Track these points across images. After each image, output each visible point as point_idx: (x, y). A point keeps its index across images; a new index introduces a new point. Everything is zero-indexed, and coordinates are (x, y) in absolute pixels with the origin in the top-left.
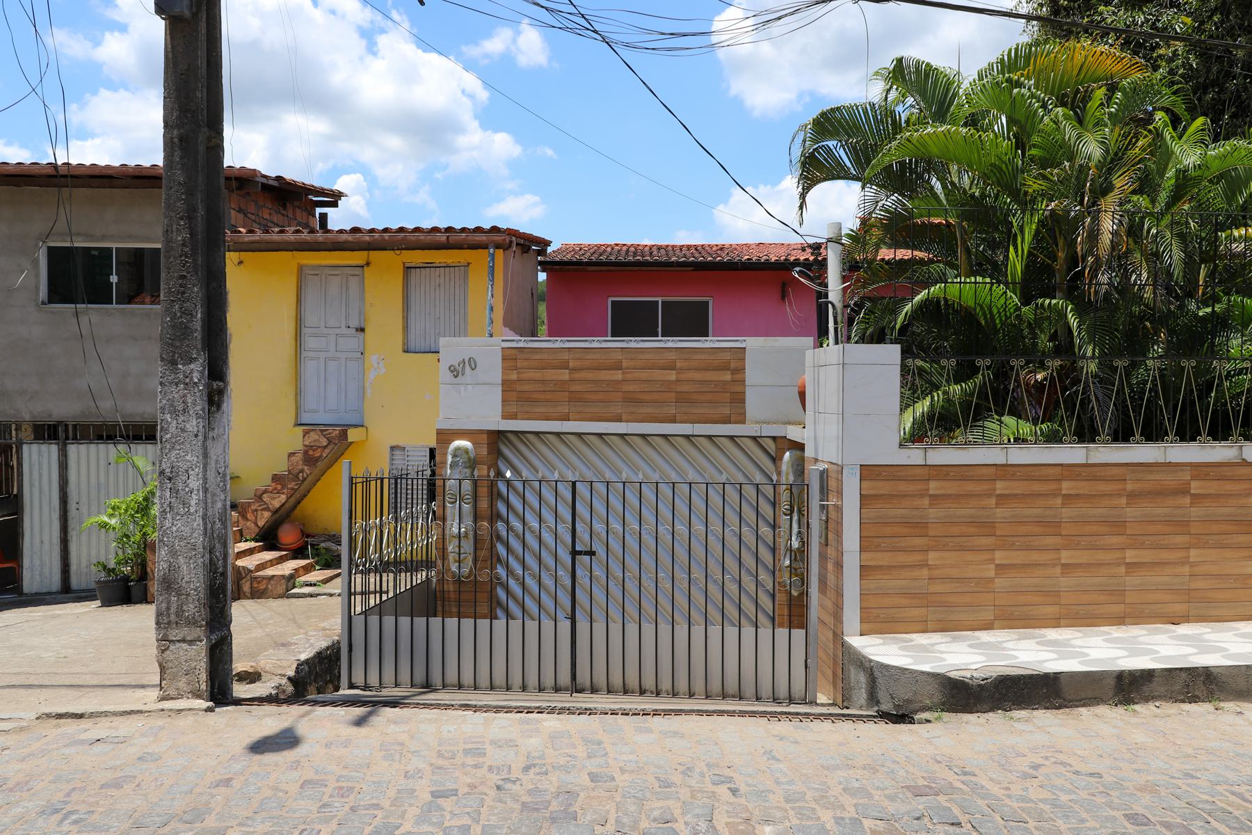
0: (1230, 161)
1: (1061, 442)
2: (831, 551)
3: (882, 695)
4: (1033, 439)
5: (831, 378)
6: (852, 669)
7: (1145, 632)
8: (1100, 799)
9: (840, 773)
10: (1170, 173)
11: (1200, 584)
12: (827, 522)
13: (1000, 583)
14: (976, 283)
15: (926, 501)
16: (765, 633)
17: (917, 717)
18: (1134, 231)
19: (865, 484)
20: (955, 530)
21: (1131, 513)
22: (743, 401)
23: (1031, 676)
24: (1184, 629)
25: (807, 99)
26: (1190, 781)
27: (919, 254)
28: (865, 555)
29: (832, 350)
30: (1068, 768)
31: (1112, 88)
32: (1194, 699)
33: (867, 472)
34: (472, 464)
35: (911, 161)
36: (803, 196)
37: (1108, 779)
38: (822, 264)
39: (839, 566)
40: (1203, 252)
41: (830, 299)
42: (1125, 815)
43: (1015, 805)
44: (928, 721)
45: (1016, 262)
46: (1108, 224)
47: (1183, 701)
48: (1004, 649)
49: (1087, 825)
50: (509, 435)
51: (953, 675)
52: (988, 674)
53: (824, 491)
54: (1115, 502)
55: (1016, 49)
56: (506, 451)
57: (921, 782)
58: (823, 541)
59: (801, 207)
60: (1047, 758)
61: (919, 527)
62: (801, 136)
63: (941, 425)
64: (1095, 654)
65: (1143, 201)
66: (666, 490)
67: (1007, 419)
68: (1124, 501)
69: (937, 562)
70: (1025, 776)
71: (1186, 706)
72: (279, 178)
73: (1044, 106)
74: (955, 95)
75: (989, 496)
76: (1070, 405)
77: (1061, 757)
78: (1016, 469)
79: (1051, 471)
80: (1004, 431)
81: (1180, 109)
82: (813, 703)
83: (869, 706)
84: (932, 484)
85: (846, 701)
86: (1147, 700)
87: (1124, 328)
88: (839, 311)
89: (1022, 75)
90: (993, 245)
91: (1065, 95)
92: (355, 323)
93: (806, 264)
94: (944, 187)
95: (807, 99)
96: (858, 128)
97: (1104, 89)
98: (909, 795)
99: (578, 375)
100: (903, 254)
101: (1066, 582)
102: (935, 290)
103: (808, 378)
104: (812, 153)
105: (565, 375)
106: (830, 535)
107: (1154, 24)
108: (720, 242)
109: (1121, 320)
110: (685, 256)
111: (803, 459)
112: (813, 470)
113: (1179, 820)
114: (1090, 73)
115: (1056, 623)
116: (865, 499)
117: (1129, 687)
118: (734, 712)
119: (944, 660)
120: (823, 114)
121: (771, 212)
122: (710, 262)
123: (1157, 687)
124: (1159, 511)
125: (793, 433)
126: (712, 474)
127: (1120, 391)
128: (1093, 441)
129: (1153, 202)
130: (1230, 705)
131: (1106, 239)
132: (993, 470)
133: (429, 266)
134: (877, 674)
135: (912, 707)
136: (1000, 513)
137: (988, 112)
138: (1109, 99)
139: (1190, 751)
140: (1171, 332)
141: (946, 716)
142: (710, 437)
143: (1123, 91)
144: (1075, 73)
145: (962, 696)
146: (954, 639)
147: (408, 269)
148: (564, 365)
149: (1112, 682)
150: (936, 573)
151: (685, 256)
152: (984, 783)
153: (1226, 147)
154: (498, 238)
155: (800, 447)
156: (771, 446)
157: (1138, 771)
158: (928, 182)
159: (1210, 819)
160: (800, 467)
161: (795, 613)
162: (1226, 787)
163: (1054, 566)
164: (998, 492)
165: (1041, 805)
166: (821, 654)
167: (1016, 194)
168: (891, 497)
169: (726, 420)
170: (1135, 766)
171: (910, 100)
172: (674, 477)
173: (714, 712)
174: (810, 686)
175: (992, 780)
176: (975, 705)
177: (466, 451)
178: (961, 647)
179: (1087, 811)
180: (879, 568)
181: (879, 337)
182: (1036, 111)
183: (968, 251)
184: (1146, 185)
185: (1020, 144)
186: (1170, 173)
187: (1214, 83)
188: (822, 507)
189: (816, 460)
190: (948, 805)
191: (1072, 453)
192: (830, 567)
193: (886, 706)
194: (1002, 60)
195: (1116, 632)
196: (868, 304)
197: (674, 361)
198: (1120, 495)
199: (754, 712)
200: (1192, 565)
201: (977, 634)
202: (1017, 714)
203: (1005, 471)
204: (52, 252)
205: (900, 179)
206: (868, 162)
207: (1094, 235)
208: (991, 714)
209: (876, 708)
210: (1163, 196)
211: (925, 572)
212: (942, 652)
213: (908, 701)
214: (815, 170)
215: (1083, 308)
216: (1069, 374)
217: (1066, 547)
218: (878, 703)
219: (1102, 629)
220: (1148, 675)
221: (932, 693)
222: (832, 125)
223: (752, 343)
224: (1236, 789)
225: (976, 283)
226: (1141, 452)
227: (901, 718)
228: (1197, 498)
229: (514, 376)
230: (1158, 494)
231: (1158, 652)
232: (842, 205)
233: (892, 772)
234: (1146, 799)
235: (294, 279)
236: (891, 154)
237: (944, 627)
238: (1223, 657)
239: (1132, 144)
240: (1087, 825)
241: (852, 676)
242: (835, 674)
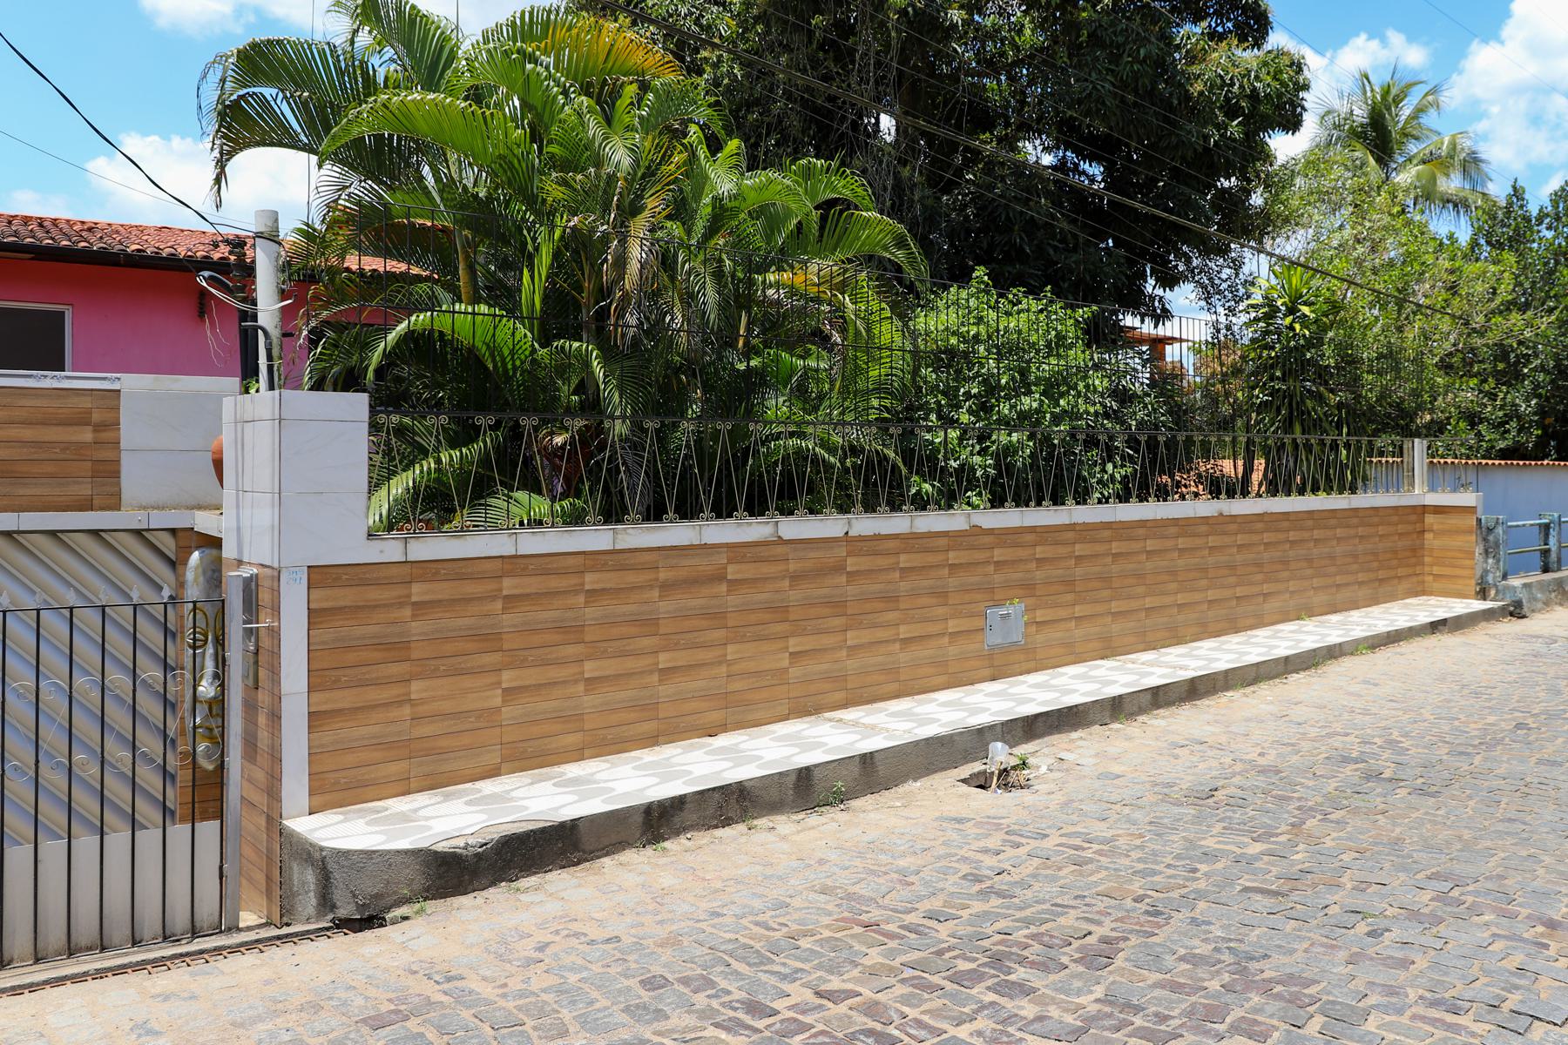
0: (767, 196)
1: (583, 523)
2: (263, 697)
3: (339, 895)
4: (550, 520)
5: (261, 440)
6: (295, 867)
7: (679, 751)
8: (615, 969)
9: (261, 1027)
10: (707, 200)
11: (737, 685)
12: (256, 653)
14: (474, 314)
17: (388, 916)
18: (667, 261)
19: (316, 594)
21: (665, 606)
22: (116, 474)
23: (543, 830)
24: (722, 740)
25: (252, 18)
26: (716, 920)
27: (415, 271)
28: (316, 697)
29: (263, 398)
30: (583, 939)
31: (644, 87)
32: (727, 822)
33: (319, 576)
35: (391, 136)
36: (221, 164)
37: (627, 940)
38: (249, 270)
39: (275, 717)
40: (739, 298)
41: (260, 322)
42: (641, 982)
43: (511, 1005)
44: (406, 918)
45: (531, 288)
46: (636, 253)
47: (716, 827)
48: (512, 800)
49: (597, 1005)
51: (440, 847)
52: (489, 837)
53: (251, 606)
54: (647, 595)
55: (531, 13)
57: (386, 1007)
58: (250, 682)
59: (218, 181)
60: (557, 932)
61: (397, 648)
62: (214, 77)
63: (433, 506)
64: (621, 787)
65: (676, 229)
66: (55, 624)
67: (521, 495)
68: (656, 593)
69: (424, 695)
70: (529, 962)
71: (719, 832)
73: (565, 93)
74: (452, 57)
76: (594, 473)
77: (576, 927)
78: (439, 566)
79: (571, 561)
80: (513, 509)
81: (717, 128)
82: (234, 928)
83: (320, 914)
84: (589, 577)
85: (286, 913)
86: (677, 833)
87: (659, 382)
88: (275, 341)
89: (538, 48)
90: (505, 265)
91: (590, 84)
93: (221, 266)
94: (438, 179)
95: (252, 18)
96: (310, 73)
97: (635, 86)
98: (365, 1030)
100: (373, 263)
102: (421, 319)
103: (227, 439)
104: (237, 102)
106: (262, 673)
107: (698, 19)
108: (89, 218)
109: (657, 368)
110: (16, 234)
111: (220, 558)
112: (234, 576)
113: (699, 971)
114: (618, 63)
115: (578, 754)
116: (315, 616)
117: (658, 822)
118: (86, 974)
119: (430, 828)
120: (254, 46)
121: (160, 182)
122: (65, 248)
123: (689, 816)
124: (460, 622)
125: (204, 522)
127: (652, 461)
128: (619, 521)
129: (689, 232)
130: (762, 822)
131: (633, 267)
132: (499, 563)
134: (331, 866)
135: (382, 903)
136: (509, 620)
137: (496, 88)
138: (640, 100)
139: (719, 885)
140: (706, 388)
141: (431, 905)
142: (53, 534)
143: (656, 93)
144: (602, 58)
145: (451, 874)
146: (447, 797)
149: (639, 819)
150: (422, 710)
151: (16, 234)
152: (473, 986)
153: (761, 177)
155: (215, 543)
156: (168, 544)
157: (661, 922)
158: (418, 171)
159: (731, 961)
160: (214, 574)
161: (205, 796)
162: (751, 918)
163: (576, 682)
164: (505, 593)
165: (544, 997)
166: (247, 851)
167: (532, 201)
169: (86, 505)
170: (659, 918)
171: (389, 52)
172: (106, 595)
173: (46, 982)
174: (228, 903)
175: (484, 979)
176: (471, 882)
178: (457, 805)
179: (599, 988)
181: (349, 381)
182: (555, 97)
183: (471, 269)
184: (681, 210)
185: (535, 136)
186: (707, 200)
187: (757, 102)
188: (249, 633)
189: (240, 562)
190: (422, 1030)
191: (596, 538)
192: (262, 720)
193: (342, 913)
194: (514, 22)
195: (647, 756)
196: (330, 334)
197: (89, 412)
198: (651, 587)
199: (124, 966)
200: (729, 663)
201: (479, 784)
202: (524, 883)
203: (514, 564)
205: (376, 158)
206: (328, 129)
207: (621, 262)
208: (491, 890)
209: (330, 916)
210: (700, 226)
211: (407, 711)
212: (428, 818)
213: (378, 896)
214: (239, 127)
215: (610, 354)
216: (592, 439)
217: (665, 649)
218: (333, 907)
219: (633, 754)
220: (679, 802)
221: (414, 875)
222: (269, 62)
223: (131, 384)
224: (760, 918)
225: (474, 314)
226: (675, 533)
227: (369, 920)
228: (734, 584)
230: (821, 572)
231: (690, 773)
232: (284, 188)
233: (345, 1003)
234: (667, 955)
236: (362, 121)
237: (433, 783)
238: (758, 767)
239: (666, 158)
240: (597, 1005)
241: (295, 876)
242: (269, 878)
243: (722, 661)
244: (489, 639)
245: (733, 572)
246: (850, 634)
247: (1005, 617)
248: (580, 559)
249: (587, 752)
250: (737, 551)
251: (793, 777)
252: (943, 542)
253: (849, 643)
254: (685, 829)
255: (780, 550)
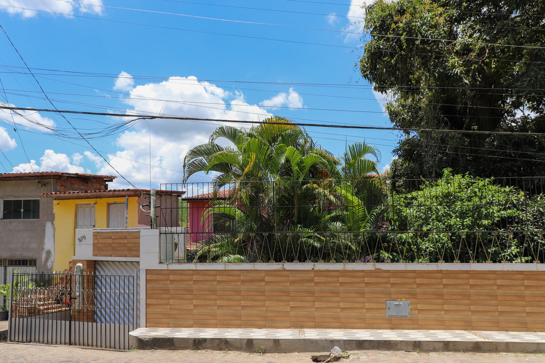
11: (269, 314)
13: (195, 311)
15: (169, 282)
16: (59, 322)
20: (156, 292)
23: (164, 339)
32: (221, 349)
34: (82, 271)
50: (100, 262)
56: (98, 267)
61: (166, 291)
66: (117, 278)
72: (76, 174)
75: (191, 280)
79: (212, 272)
92: (93, 224)
99: (114, 241)
101: (218, 312)
105: (110, 241)
126: (125, 273)
133: (115, 203)
147: (109, 205)
148: (110, 238)
149: (192, 342)
154: (128, 193)
168: (180, 281)
172: (120, 274)
177: (80, 267)
180: (153, 304)
200: (266, 307)
204: (5, 202)
220: (205, 340)
228: (317, 283)
229: (96, 242)
235: (74, 209)
243: (264, 306)
244: (190, 291)
245: (267, 279)
246: (316, 303)
247: (397, 305)
248: (215, 272)
249: (218, 326)
250: (268, 272)
251: (246, 341)
252: (360, 274)
253: (316, 306)
254: (207, 348)
255: (285, 273)
